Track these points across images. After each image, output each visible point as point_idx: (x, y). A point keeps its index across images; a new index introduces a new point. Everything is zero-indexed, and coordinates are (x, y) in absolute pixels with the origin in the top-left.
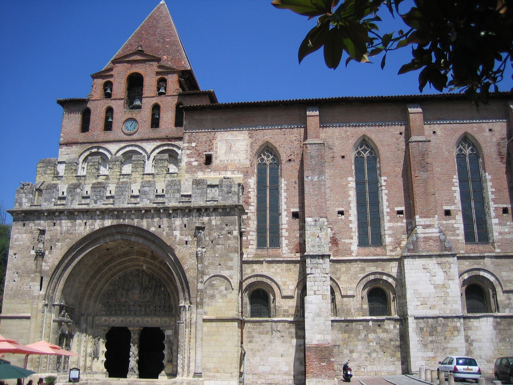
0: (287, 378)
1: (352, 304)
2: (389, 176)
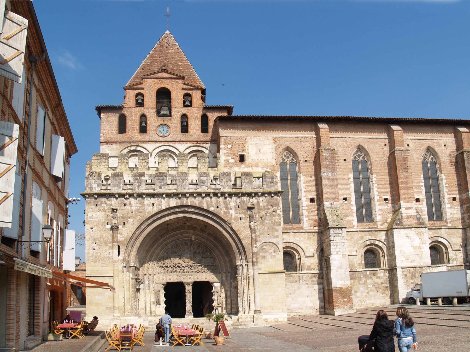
0: (312, 311)
1: (355, 260)
2: (378, 174)
